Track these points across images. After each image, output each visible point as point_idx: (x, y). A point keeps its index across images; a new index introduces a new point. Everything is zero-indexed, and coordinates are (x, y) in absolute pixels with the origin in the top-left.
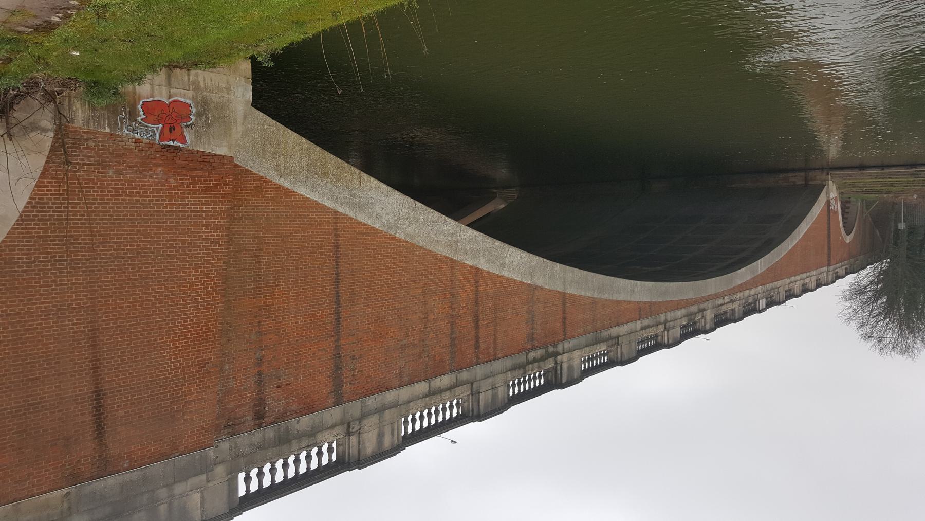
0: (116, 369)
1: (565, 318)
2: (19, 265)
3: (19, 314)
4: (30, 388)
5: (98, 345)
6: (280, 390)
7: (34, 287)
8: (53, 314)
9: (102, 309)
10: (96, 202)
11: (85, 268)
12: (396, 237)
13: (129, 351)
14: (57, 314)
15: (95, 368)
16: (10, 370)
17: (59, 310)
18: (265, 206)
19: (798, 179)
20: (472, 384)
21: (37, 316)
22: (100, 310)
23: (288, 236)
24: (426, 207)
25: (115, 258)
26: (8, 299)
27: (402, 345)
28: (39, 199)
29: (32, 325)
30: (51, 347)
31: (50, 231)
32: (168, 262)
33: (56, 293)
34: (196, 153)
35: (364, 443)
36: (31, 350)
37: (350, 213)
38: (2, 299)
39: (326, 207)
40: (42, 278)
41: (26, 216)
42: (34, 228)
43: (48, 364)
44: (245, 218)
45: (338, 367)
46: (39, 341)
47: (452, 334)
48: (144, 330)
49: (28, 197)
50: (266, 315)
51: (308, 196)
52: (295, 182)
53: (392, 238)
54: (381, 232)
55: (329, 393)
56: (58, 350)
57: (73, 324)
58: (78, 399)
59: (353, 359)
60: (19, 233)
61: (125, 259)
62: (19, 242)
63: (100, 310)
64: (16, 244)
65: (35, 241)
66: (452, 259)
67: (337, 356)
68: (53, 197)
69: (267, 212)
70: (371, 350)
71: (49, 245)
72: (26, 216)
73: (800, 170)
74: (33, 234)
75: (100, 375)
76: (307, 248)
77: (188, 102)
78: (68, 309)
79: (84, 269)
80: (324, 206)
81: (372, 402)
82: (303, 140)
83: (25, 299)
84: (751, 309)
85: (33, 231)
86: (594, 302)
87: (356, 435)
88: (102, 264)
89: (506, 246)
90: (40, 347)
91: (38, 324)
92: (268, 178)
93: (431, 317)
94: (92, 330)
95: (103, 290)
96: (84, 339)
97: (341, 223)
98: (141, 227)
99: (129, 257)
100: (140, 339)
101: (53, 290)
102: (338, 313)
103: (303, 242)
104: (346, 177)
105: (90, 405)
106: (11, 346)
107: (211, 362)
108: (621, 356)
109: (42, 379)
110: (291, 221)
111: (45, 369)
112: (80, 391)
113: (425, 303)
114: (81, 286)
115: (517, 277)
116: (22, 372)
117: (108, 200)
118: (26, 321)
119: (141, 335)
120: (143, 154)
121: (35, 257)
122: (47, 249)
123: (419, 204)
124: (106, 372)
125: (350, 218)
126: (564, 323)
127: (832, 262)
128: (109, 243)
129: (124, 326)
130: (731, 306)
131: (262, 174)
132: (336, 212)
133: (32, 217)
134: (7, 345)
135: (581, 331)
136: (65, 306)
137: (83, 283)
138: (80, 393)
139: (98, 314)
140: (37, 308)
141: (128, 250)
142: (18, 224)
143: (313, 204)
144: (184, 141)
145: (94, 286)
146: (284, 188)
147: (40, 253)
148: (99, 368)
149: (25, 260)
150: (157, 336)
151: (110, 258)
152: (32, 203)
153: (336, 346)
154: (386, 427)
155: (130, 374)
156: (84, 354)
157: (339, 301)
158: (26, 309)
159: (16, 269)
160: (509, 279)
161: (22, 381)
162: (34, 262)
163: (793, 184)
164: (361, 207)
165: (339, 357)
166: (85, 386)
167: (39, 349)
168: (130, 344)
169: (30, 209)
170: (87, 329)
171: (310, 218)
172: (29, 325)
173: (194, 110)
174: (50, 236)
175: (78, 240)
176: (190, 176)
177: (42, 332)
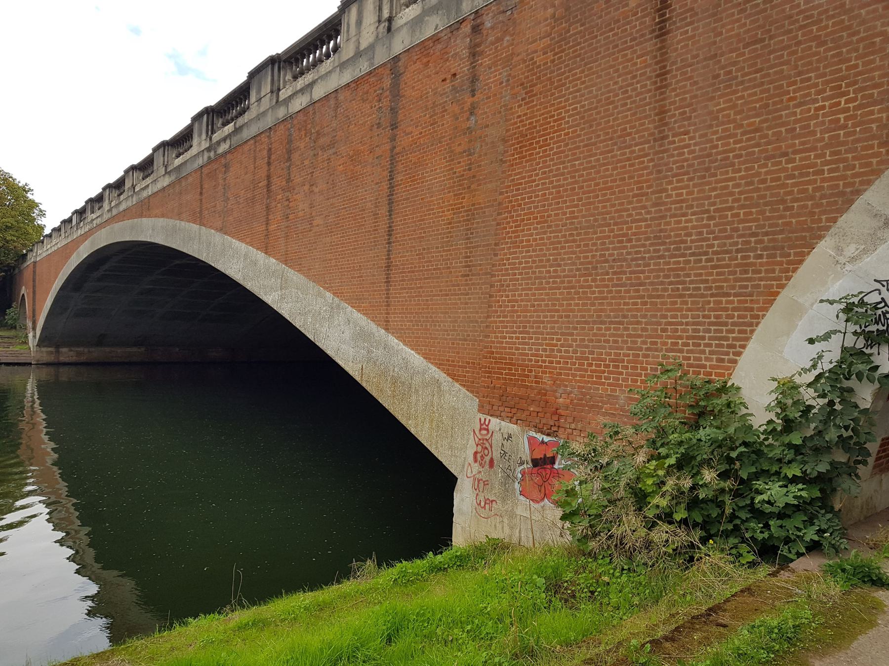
0: (634, 77)
1: (201, 193)
2: (762, 245)
3: (767, 158)
4: (759, 27)
5: (656, 115)
6: (453, 71)
7: (742, 207)
8: (716, 161)
9: (648, 174)
10: (644, 352)
11: (666, 242)
12: (334, 294)
13: (616, 108)
14: (711, 162)
15: (663, 74)
16: (789, 54)
17: (708, 169)
18: (456, 339)
19: (67, 354)
20: (277, 101)
21: (741, 156)
22: (651, 173)
23: (434, 296)
24: (305, 333)
25: (625, 260)
26: (784, 184)
27: (334, 147)
28: (722, 360)
29: (748, 140)
30: (724, 103)
31: (712, 305)
32: (560, 254)
33: (710, 197)
34: (519, 421)
35: (375, 8)
36: (755, 94)
37: (373, 327)
38: (792, 183)
39: (395, 337)
40: (728, 223)
41: (745, 332)
42: (734, 309)
43: (730, 72)
44: (477, 322)
45: (393, 111)
46: (741, 112)
47: (290, 166)
48: (595, 144)
49: (740, 363)
50: (463, 180)
51: (412, 352)
52: (424, 372)
53: (337, 293)
54: (346, 301)
55: (404, 72)
56: (713, 98)
57: (688, 146)
58: (691, 17)
59: (379, 123)
60: (757, 302)
61: (613, 258)
62: (758, 286)
63: (651, 173)
64: (762, 283)
65: (733, 287)
66: (286, 264)
67: (394, 126)
68: (703, 362)
69: (455, 330)
70: (362, 138)
71: (714, 281)
72: (745, 332)
73: (65, 364)
74: (736, 299)
75: (657, 63)
76: (417, 279)
77: (522, 498)
78: (695, 171)
79: (668, 241)
80: (397, 338)
81: (364, 67)
82: (413, 431)
83: (756, 185)
84: (80, 213)
85: (736, 305)
86: (179, 216)
87: (383, 19)
88: (642, 249)
89: (241, 282)
90: (740, 102)
91: (741, 141)
92: (451, 380)
93: (306, 187)
94: (663, 138)
95: (644, 207)
96: (675, 122)
97: (382, 314)
98: (589, 310)
99: (607, 261)
100: (601, 130)
101: (714, 204)
102: (391, 187)
103: (421, 287)
104: (374, 377)
105: (675, 10)
106: (785, 98)
107: (519, 101)
108: (164, 152)
109: (741, 45)
110: (431, 317)
111: (735, 63)
112: (687, 32)
113: (311, 206)
114: (673, 211)
115: (236, 243)
116: (770, 53)
117: (628, 355)
118: (758, 145)
119: (599, 136)
120: (579, 426)
121: (737, 260)
122: (718, 274)
123: (311, 337)
124: (648, 70)
125: (374, 321)
126: (202, 189)
127: (31, 266)
128: (632, 285)
129: (620, 149)
130: (94, 216)
131: (457, 385)
132: (387, 329)
133: (736, 329)
134: (791, 99)
135: (190, 179)
136: (698, 176)
137: (671, 217)
138: (686, 29)
139: (654, 166)
140: (739, 171)
141: (607, 274)
142: (757, 317)
143: (409, 341)
144: (531, 440)
145: (656, 212)
146: (436, 364)
147: (728, 266)
148: (658, 76)
149: (752, 254)
150: (579, 136)
151: (632, 260)
152: (734, 354)
153: (395, 140)
154: (354, 34)
155: (617, 71)
156: (676, 96)
157: (389, 204)
158: (756, 167)
159: (766, 238)
160: (241, 240)
161: (771, 38)
162: (738, 251)
163: (73, 349)
164: (362, 336)
165: (392, 125)
166: (679, 42)
167: (742, 97)
168: (614, 120)
169: (738, 344)
170: (671, 139)
171: (412, 321)
172: (753, 138)
173: (517, 486)
174: (712, 295)
175: (673, 290)
176: (527, 387)
177: (735, 128)
